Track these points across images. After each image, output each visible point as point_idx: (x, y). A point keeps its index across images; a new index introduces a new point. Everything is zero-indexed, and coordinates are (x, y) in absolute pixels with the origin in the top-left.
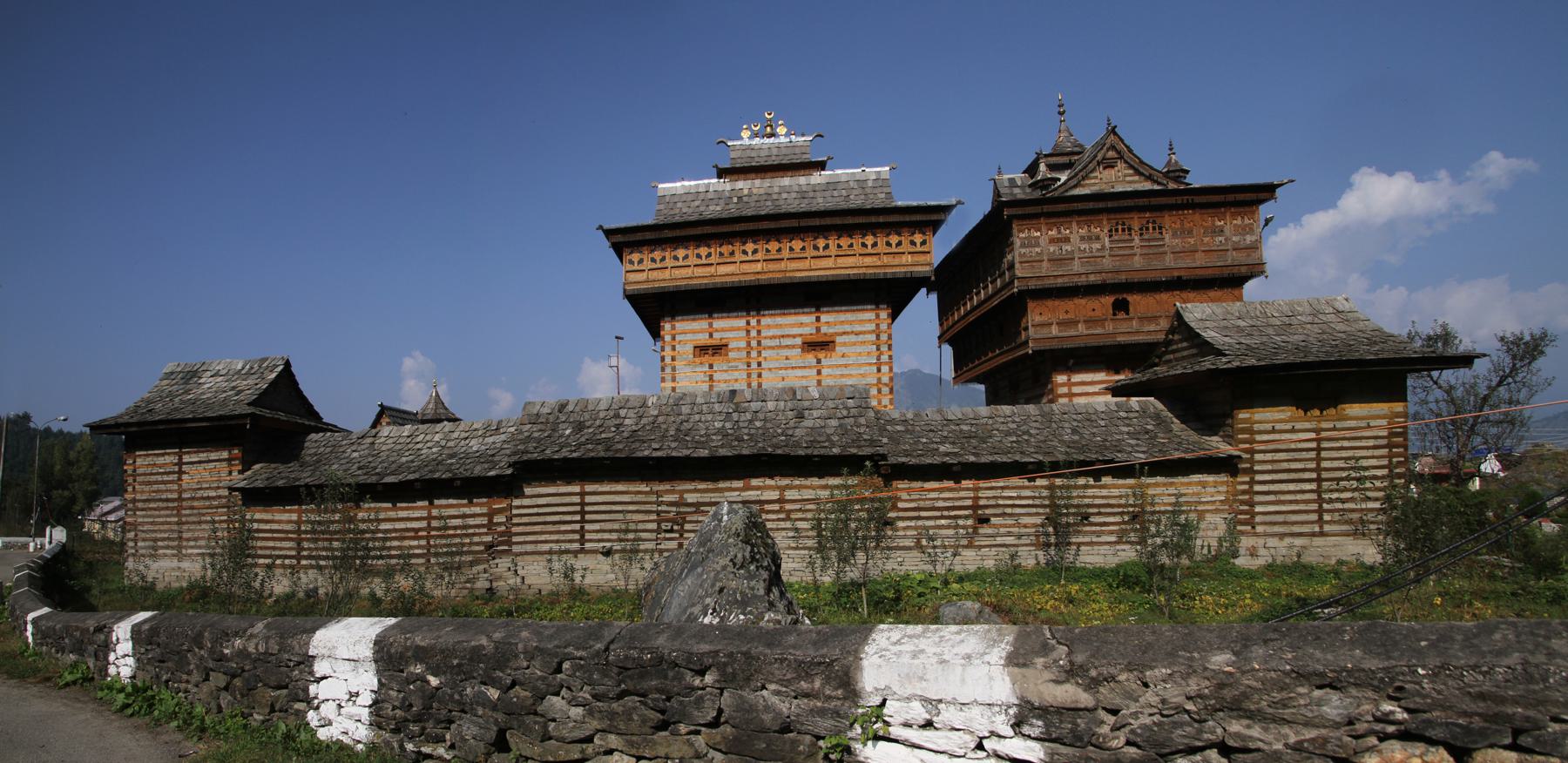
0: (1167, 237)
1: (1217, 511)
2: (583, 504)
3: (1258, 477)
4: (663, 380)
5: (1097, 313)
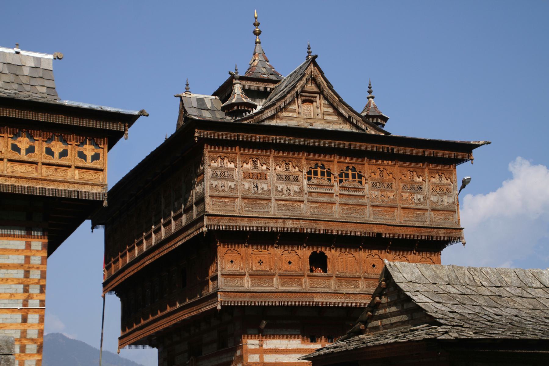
0: (367, 187)
5: (294, 267)
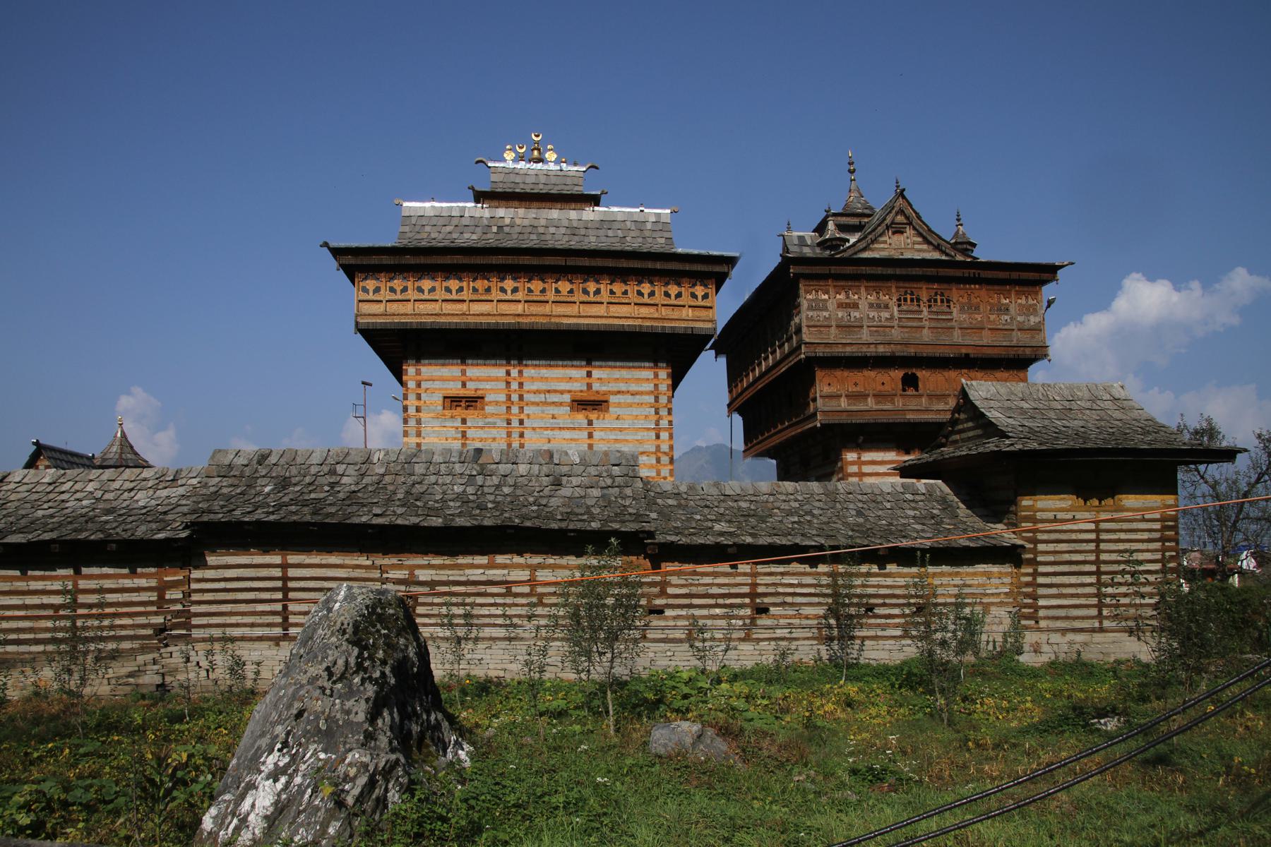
0: (955, 311)
1: (1001, 604)
2: (285, 579)
3: (1041, 569)
4: (406, 434)
5: (887, 388)
